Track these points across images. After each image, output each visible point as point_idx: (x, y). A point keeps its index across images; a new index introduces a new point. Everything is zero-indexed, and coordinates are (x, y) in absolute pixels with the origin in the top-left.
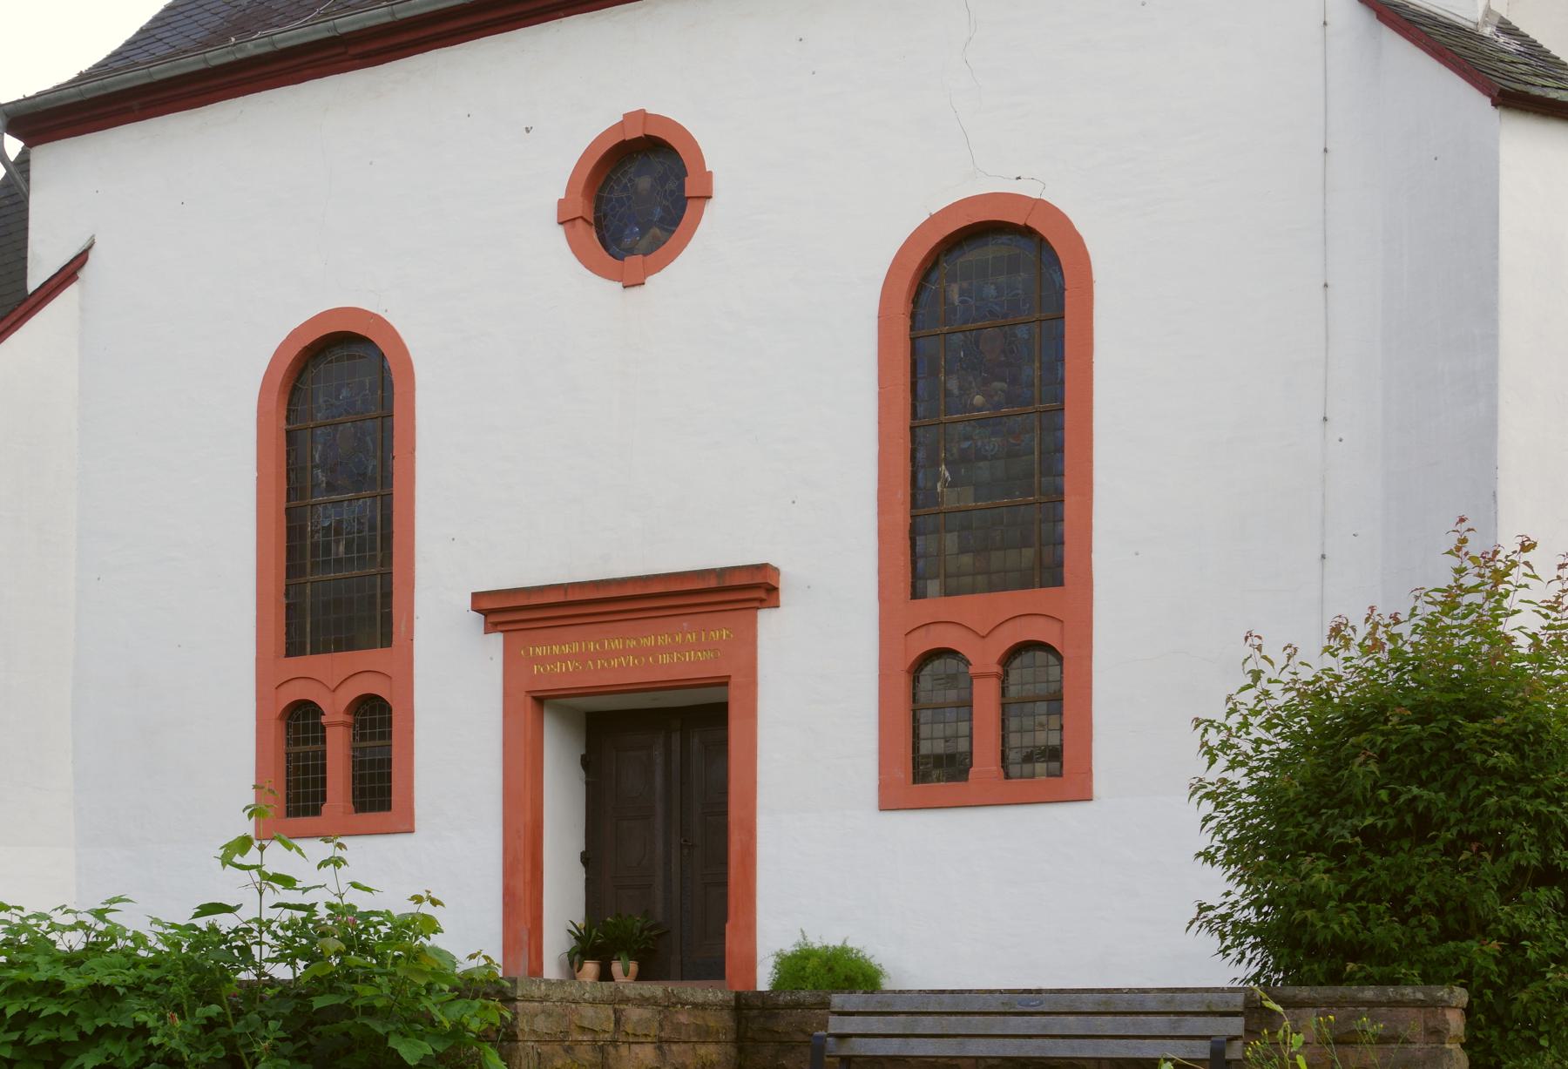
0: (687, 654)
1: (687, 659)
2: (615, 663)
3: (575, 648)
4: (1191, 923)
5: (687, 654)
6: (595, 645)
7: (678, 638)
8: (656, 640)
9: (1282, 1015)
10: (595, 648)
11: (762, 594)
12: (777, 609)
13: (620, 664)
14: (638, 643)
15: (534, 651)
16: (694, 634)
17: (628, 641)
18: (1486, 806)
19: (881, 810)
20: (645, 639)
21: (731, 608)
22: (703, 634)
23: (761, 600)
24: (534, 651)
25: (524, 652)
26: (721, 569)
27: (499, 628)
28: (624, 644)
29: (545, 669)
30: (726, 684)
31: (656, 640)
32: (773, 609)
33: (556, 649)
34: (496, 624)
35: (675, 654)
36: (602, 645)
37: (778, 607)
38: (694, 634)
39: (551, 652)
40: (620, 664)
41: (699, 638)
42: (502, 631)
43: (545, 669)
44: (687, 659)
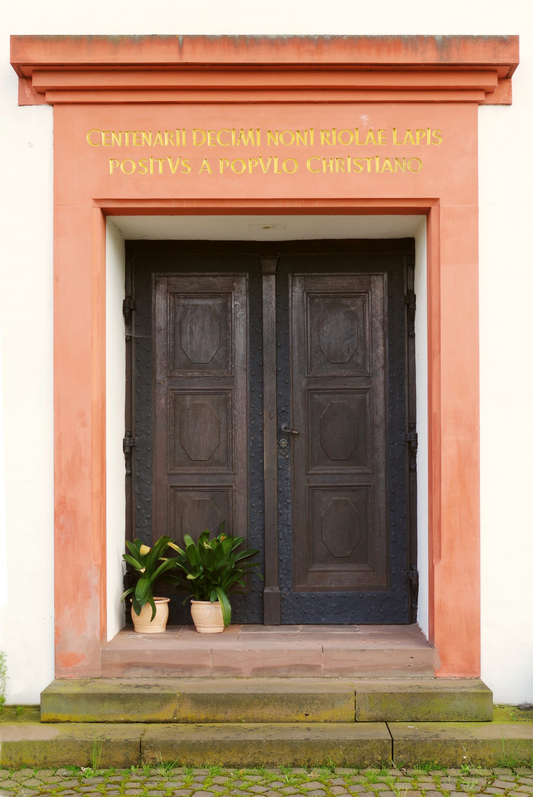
0: (369, 162)
1: (369, 170)
2: (248, 167)
3: (181, 138)
4: (92, 499)
5: (369, 162)
6: (214, 136)
7: (354, 138)
8: (317, 138)
9: (345, 132)
10: (214, 142)
11: (490, 81)
12: (508, 107)
13: (257, 170)
14: (287, 138)
15: (109, 137)
16: (379, 134)
17: (269, 135)
18: (236, 571)
19: (20, 105)
20: (298, 135)
21: (412, 67)
22: (395, 133)
23: (488, 92)
24: (109, 137)
25: (91, 138)
26: (444, 38)
27: (50, 97)
28: (264, 139)
29: (128, 167)
30: (426, 212)
31: (317, 138)
32: (501, 108)
33: (147, 138)
34: (42, 92)
35: (349, 160)
36: (226, 138)
37: (509, 104)
38: (379, 134)
39: (139, 142)
40: (257, 170)
41: (388, 139)
42: (52, 104)
43: (128, 167)
44: (369, 170)
